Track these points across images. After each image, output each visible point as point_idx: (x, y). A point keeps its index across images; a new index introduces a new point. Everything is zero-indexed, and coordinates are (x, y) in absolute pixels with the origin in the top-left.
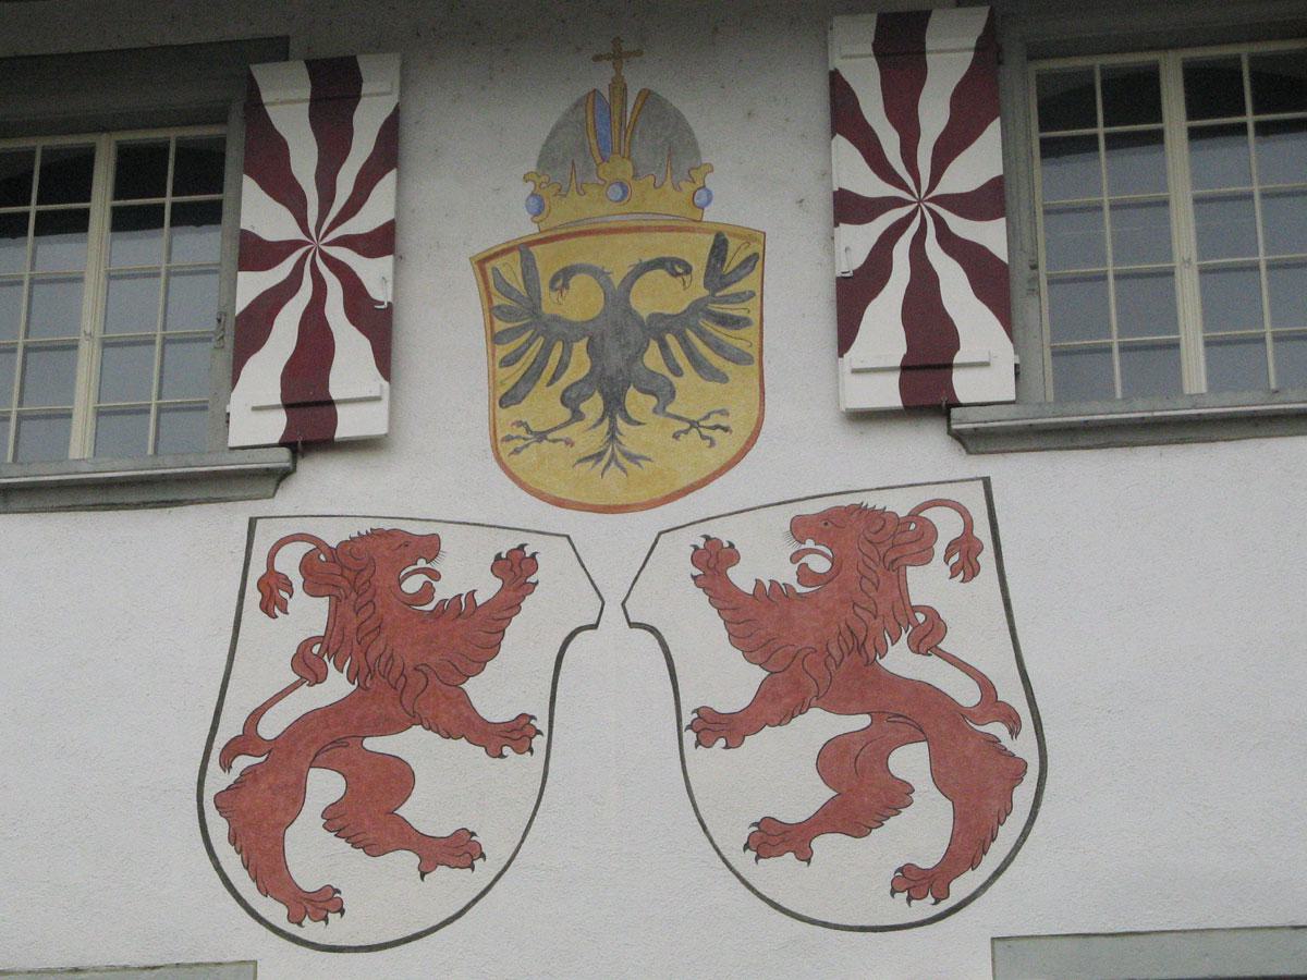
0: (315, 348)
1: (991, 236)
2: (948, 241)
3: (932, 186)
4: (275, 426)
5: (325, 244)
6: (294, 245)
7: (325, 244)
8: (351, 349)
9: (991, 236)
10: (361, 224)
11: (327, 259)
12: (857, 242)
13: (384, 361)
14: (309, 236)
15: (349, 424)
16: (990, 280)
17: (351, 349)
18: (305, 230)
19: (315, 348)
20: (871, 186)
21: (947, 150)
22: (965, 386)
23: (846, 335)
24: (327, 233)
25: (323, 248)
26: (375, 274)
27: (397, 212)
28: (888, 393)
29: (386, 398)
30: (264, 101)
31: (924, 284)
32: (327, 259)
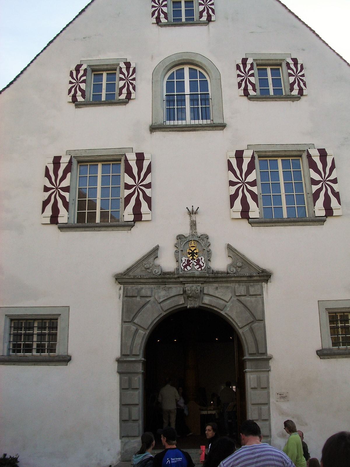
0: (138, 204)
1: (66, 195)
2: (248, 191)
3: (59, 186)
4: (131, 218)
5: (139, 186)
6: (133, 186)
7: (139, 186)
8: (334, 200)
9: (254, 189)
10: (144, 183)
11: (140, 189)
12: (233, 189)
13: (150, 207)
14: (136, 184)
15: (335, 213)
16: (254, 197)
17: (144, 205)
18: (136, 183)
19: (138, 204)
20: (236, 180)
21: (247, 174)
22: (251, 215)
23: (232, 206)
24: (139, 184)
25: (139, 186)
26: (148, 192)
27: (70, 184)
28: (48, 221)
29: (151, 213)
30: (53, 164)
31: (244, 198)
32: (140, 189)
